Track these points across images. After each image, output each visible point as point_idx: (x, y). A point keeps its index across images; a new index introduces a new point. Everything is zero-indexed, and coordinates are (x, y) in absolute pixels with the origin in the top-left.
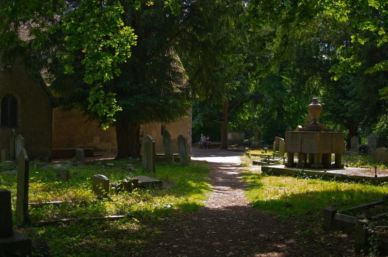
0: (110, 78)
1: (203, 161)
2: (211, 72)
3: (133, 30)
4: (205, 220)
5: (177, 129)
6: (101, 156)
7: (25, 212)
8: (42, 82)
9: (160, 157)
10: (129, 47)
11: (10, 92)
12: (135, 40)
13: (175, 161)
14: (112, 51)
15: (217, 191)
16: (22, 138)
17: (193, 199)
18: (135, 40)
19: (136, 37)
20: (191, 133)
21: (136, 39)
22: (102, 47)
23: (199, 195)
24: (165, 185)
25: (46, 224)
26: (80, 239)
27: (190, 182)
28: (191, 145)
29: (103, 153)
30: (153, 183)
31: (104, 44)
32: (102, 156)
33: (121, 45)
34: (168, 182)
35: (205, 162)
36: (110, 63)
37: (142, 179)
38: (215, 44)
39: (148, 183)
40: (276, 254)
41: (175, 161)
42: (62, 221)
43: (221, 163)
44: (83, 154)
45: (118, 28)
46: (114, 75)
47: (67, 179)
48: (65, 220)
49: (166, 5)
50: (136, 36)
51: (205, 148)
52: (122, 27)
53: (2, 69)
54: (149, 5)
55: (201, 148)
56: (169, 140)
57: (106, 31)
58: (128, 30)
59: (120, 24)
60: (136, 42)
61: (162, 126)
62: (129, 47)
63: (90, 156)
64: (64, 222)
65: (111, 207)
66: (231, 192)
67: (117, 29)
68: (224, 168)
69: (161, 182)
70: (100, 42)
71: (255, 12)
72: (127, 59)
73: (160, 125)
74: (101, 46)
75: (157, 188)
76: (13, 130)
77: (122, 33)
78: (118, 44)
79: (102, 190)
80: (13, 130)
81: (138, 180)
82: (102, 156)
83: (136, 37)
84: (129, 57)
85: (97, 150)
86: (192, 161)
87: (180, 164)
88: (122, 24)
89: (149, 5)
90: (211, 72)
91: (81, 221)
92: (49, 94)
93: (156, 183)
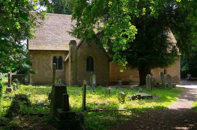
0: (125, 49)
1: (183, 87)
2: (185, 42)
3: (135, 27)
4: (164, 113)
5: (172, 71)
6: (133, 85)
7: (84, 105)
8: (104, 50)
9: (160, 85)
10: (134, 34)
11: (90, 55)
12: (136, 31)
13: (166, 87)
14: (126, 36)
15: (180, 101)
16: (95, 76)
17: (165, 105)
18: (136, 31)
19: (137, 30)
20: (180, 73)
21: (137, 31)
22: (122, 35)
23: (169, 103)
24: (154, 97)
25: (93, 111)
26: (104, 117)
27: (167, 97)
28: (180, 79)
29: (135, 83)
30: (147, 96)
31: (123, 34)
32: (134, 84)
33: (130, 33)
34: (156, 96)
35: (184, 88)
36: (125, 42)
37: (142, 95)
38: (186, 28)
39: (145, 96)
40: (185, 128)
41: (166, 87)
42: (99, 110)
43: (193, 89)
44: (121, 83)
45: (129, 26)
46: (127, 47)
47: (109, 93)
48: (101, 110)
49: (151, 14)
50: (137, 29)
51: (190, 81)
52: (130, 26)
53: (87, 45)
54: (143, 15)
55: (188, 81)
56: (163, 77)
57: (123, 28)
58: (133, 27)
59: (129, 24)
60: (137, 32)
61: (164, 70)
62: (134, 34)
63: (128, 84)
64: (100, 111)
65: (121, 107)
66: (187, 102)
67: (128, 27)
68: (192, 91)
69: (152, 96)
70: (121, 33)
71: (194, 13)
72: (134, 40)
73: (164, 69)
74: (121, 34)
75: (149, 98)
76: (92, 72)
77: (130, 28)
78: (129, 33)
79: (122, 99)
80: (92, 72)
81: (140, 95)
82: (134, 84)
83: (137, 30)
84: (134, 39)
85: (131, 82)
86: (177, 87)
87: (168, 88)
88: (131, 24)
89: (143, 15)
90: (185, 42)
91: (107, 111)
92: (107, 56)
93: (149, 97)
